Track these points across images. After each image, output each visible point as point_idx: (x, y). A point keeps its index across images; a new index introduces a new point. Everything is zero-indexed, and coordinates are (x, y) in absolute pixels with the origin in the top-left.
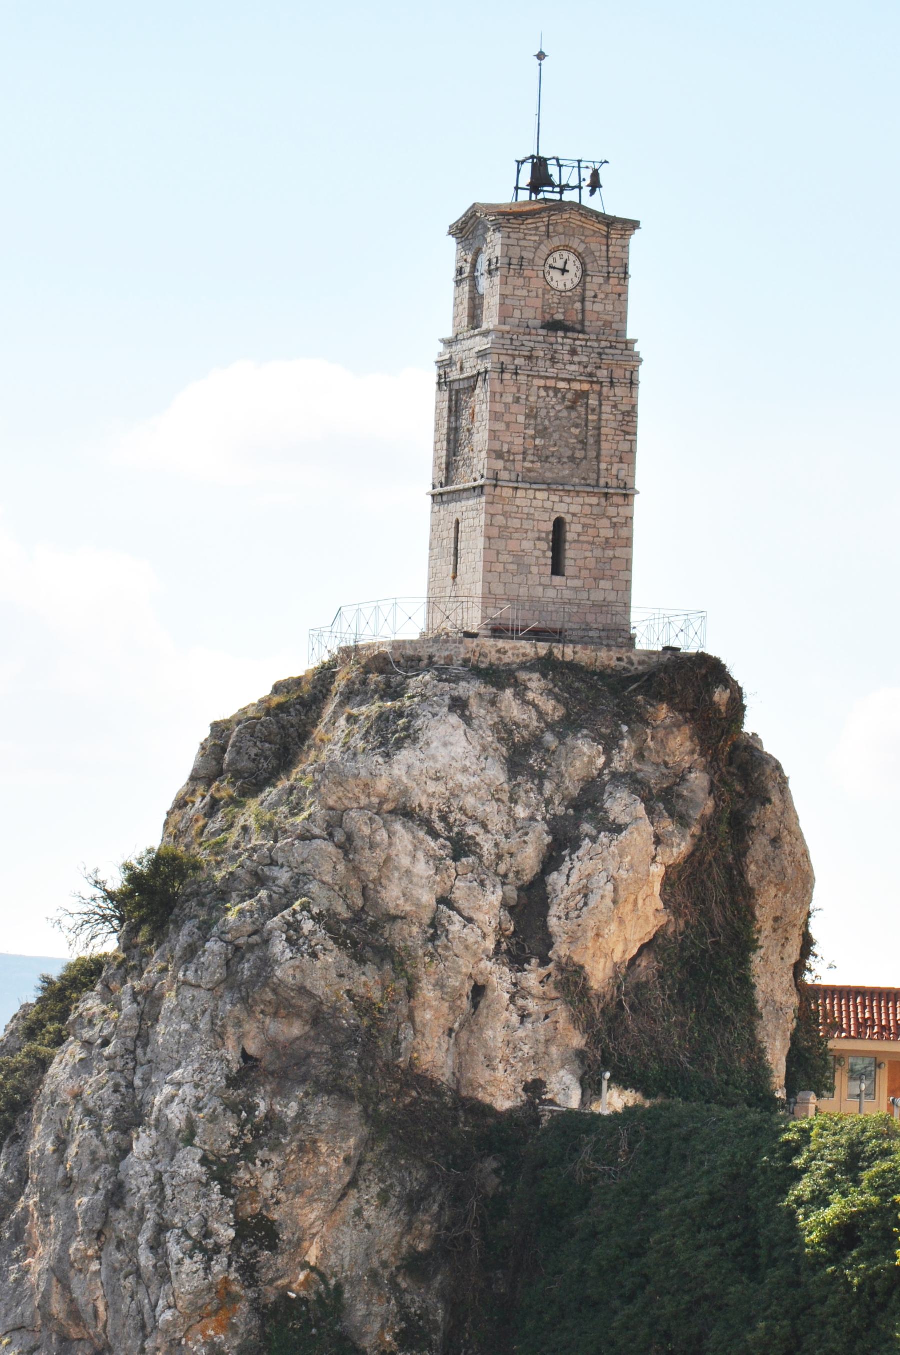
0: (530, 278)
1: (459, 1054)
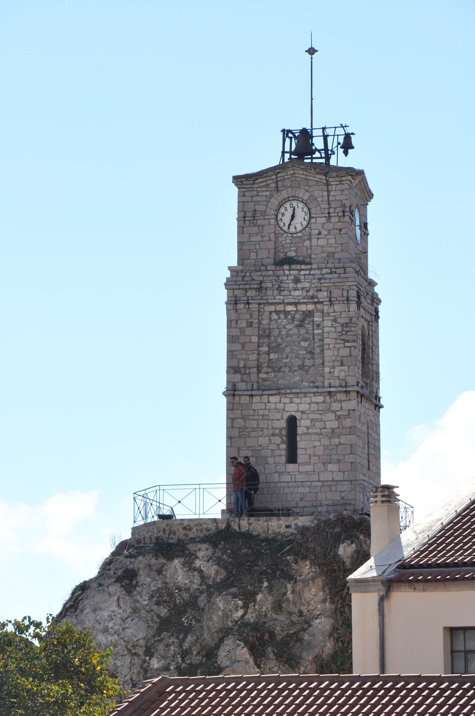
0: (263, 226)
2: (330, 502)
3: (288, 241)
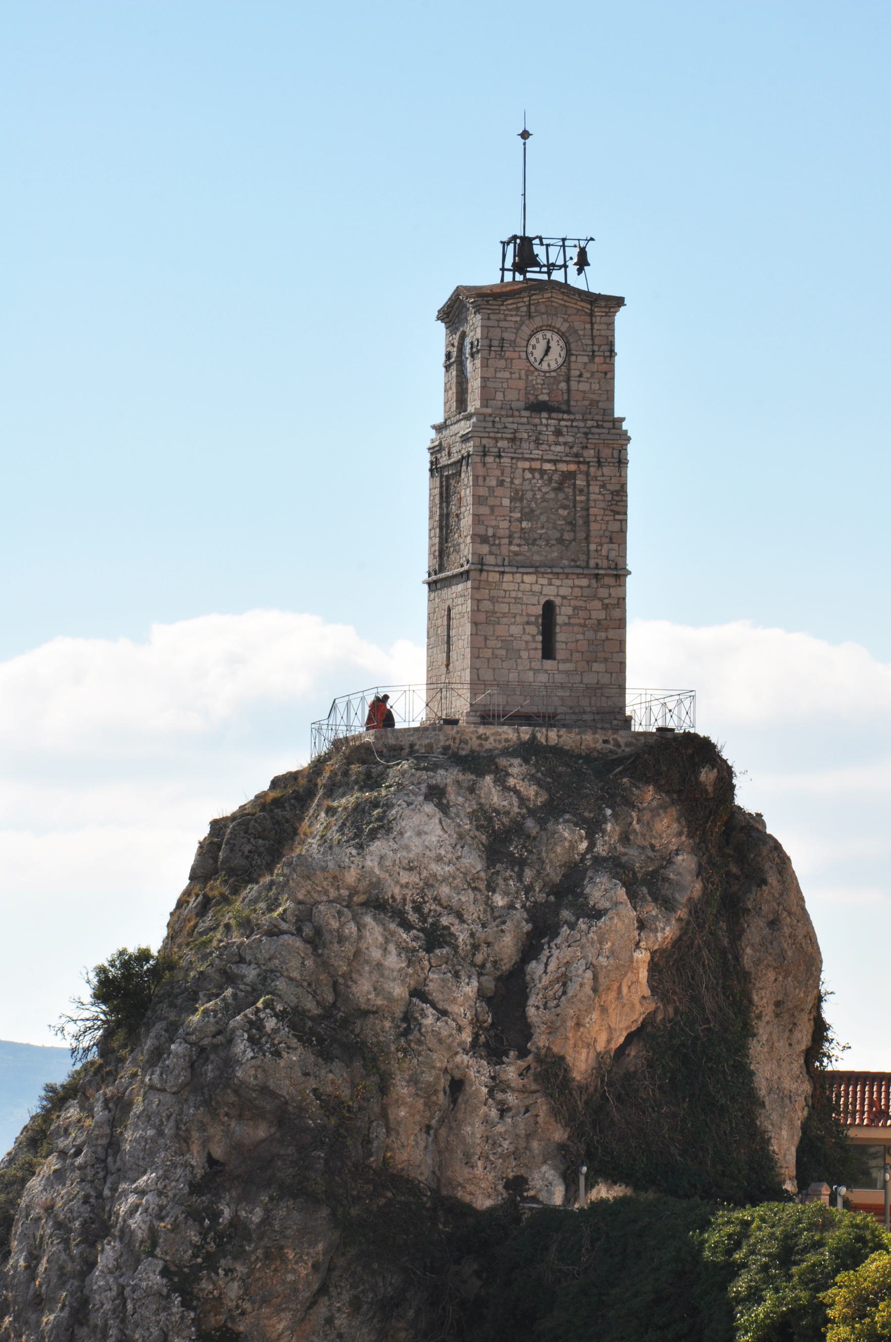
0: (512, 359)
1: (439, 1152)
2: (594, 708)
3: (539, 381)
